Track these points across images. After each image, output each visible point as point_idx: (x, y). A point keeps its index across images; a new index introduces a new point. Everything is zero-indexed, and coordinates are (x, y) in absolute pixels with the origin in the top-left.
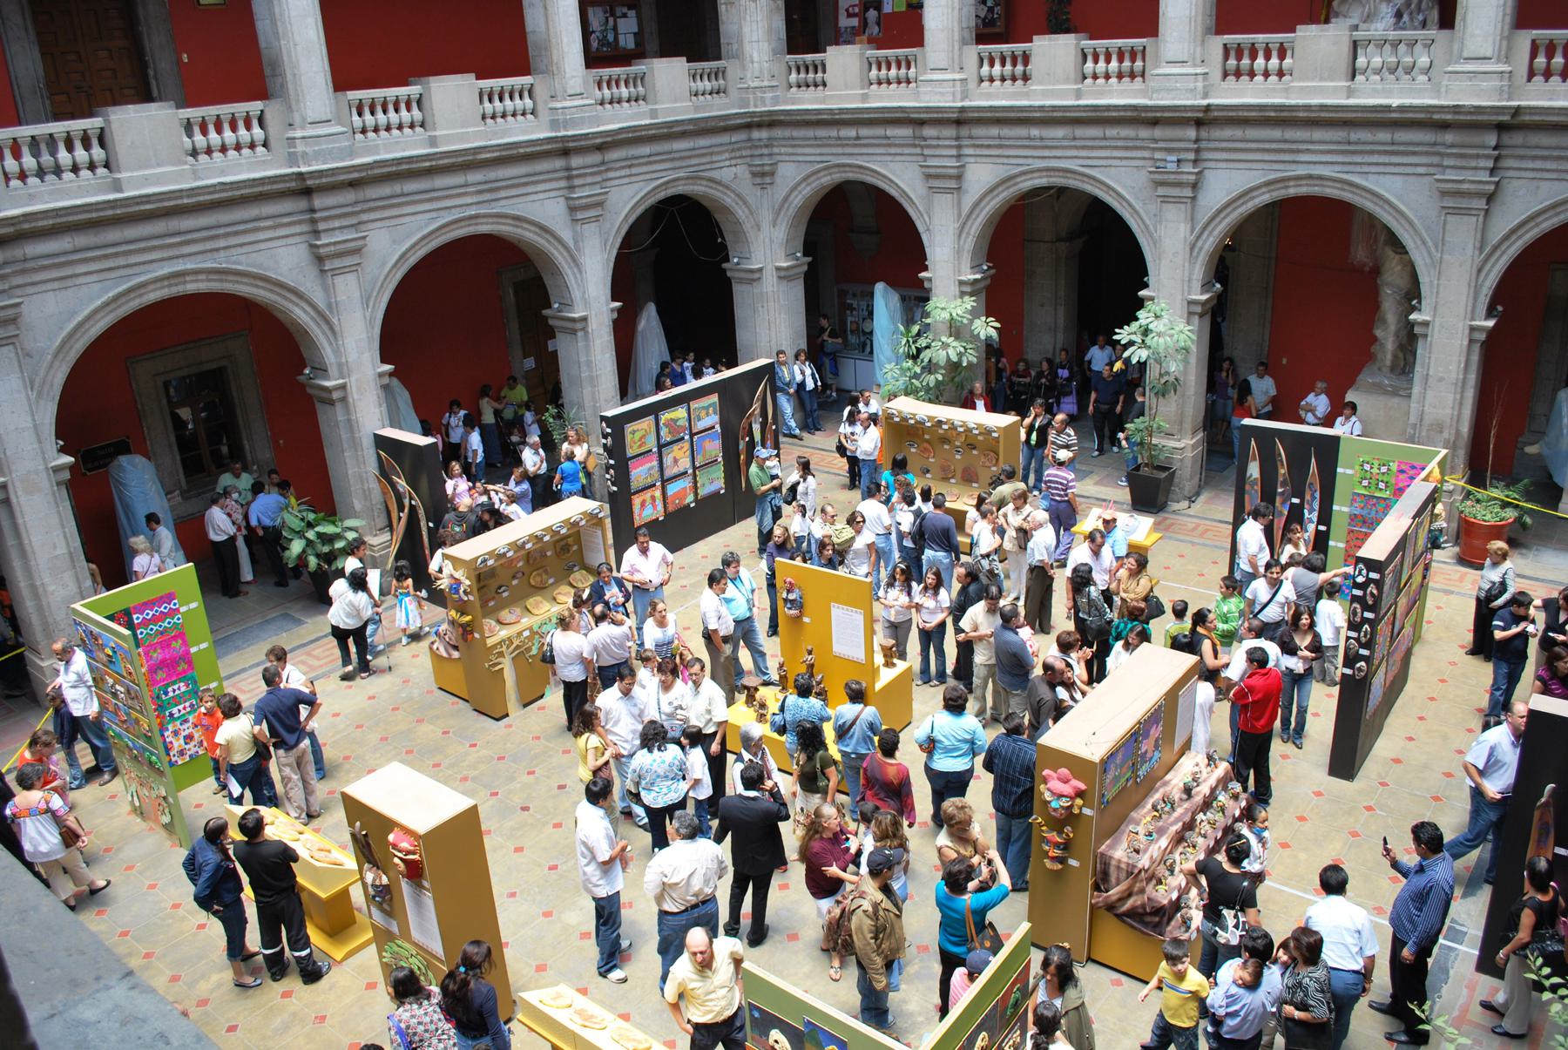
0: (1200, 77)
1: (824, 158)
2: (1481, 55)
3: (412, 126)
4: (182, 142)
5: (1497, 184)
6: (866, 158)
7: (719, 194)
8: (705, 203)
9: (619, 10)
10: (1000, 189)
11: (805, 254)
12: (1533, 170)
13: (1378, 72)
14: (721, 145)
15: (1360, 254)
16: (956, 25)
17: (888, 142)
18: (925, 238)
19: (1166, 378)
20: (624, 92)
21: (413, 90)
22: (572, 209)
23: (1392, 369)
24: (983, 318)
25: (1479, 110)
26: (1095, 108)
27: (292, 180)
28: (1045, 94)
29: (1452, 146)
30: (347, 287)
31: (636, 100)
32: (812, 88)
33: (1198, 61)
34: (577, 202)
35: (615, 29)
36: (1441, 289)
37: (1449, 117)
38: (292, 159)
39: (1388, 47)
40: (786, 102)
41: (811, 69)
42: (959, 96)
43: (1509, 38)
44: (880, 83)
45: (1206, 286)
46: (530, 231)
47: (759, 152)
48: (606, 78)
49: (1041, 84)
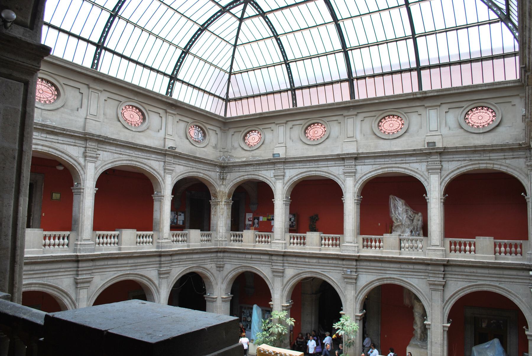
0: (356, 247)
1: (240, 264)
3: (114, 244)
4: (42, 241)
5: (445, 282)
6: (253, 264)
7: (206, 273)
8: (201, 275)
9: (179, 213)
10: (296, 277)
11: (231, 294)
12: (455, 278)
13: (408, 248)
14: (208, 257)
15: (407, 302)
16: (283, 227)
18: (271, 291)
19: (350, 341)
20: (180, 239)
21: (116, 233)
22: (159, 274)
24: (290, 318)
25: (437, 260)
26: (325, 254)
27: (74, 257)
28: (310, 249)
29: (431, 270)
30: (83, 294)
31: (183, 241)
32: (238, 242)
33: (355, 242)
35: (177, 219)
36: (433, 314)
37: (429, 262)
38: (75, 250)
39: (410, 241)
40: (229, 246)
41: (238, 236)
42: (284, 248)
43: (443, 240)
44: (259, 242)
45: (361, 311)
47: (219, 260)
48: (175, 234)
49: (309, 246)
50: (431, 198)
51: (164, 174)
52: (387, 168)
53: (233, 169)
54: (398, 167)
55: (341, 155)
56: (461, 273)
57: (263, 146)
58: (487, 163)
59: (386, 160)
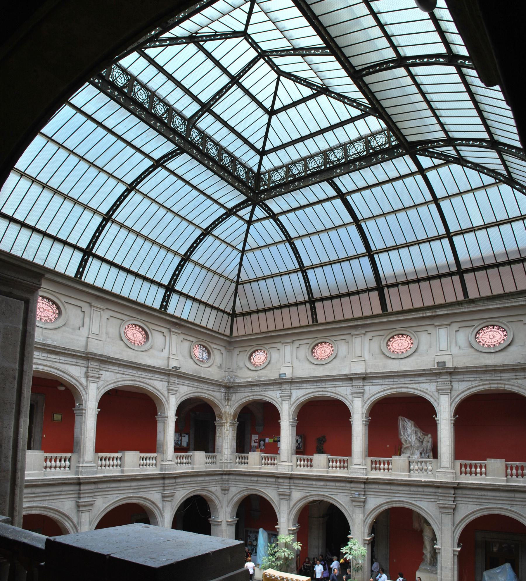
0: (365, 469)
1: (246, 486)
2: (446, 467)
3: (117, 466)
5: (456, 505)
6: (259, 487)
7: (210, 495)
9: (183, 435)
10: (303, 500)
11: (237, 517)
13: (417, 470)
14: (213, 480)
15: (416, 525)
17: (267, 483)
18: (277, 514)
19: (358, 565)
20: (184, 461)
21: (119, 455)
22: (163, 497)
23: (430, 564)
24: (296, 542)
25: (447, 483)
27: (75, 480)
28: (317, 471)
29: (441, 493)
30: (85, 517)
32: (243, 464)
33: (364, 464)
34: (165, 495)
35: (181, 440)
37: (439, 485)
38: (77, 473)
39: (419, 463)
40: (234, 468)
41: (243, 458)
43: (454, 462)
45: (369, 535)
46: (148, 503)
47: (224, 483)
50: (441, 419)
51: (168, 394)
52: (396, 388)
53: (239, 389)
54: (408, 388)
55: (349, 375)
56: (471, 496)
57: (269, 366)
58: (498, 384)
59: (395, 380)
